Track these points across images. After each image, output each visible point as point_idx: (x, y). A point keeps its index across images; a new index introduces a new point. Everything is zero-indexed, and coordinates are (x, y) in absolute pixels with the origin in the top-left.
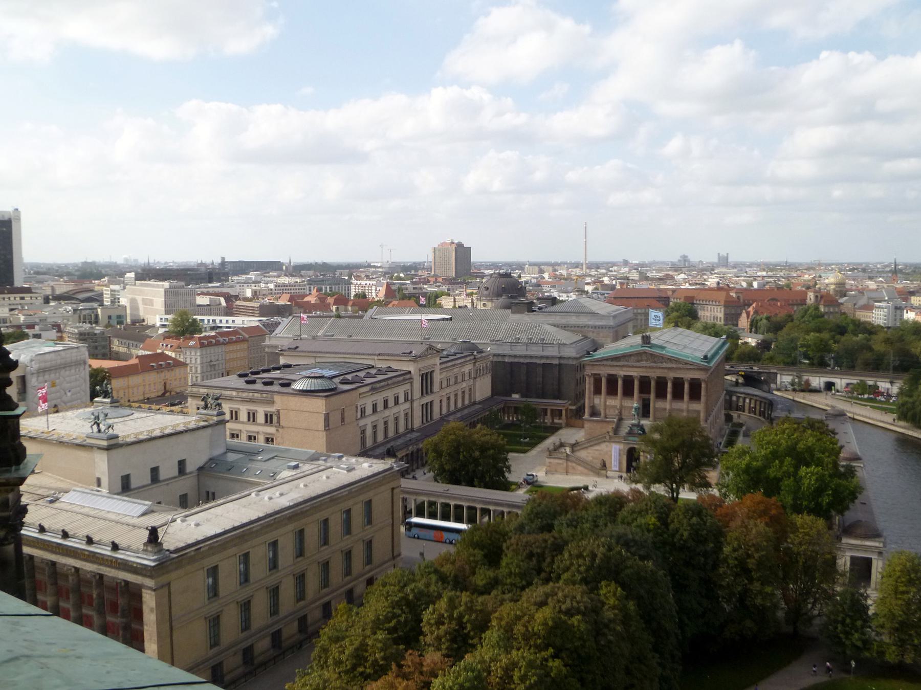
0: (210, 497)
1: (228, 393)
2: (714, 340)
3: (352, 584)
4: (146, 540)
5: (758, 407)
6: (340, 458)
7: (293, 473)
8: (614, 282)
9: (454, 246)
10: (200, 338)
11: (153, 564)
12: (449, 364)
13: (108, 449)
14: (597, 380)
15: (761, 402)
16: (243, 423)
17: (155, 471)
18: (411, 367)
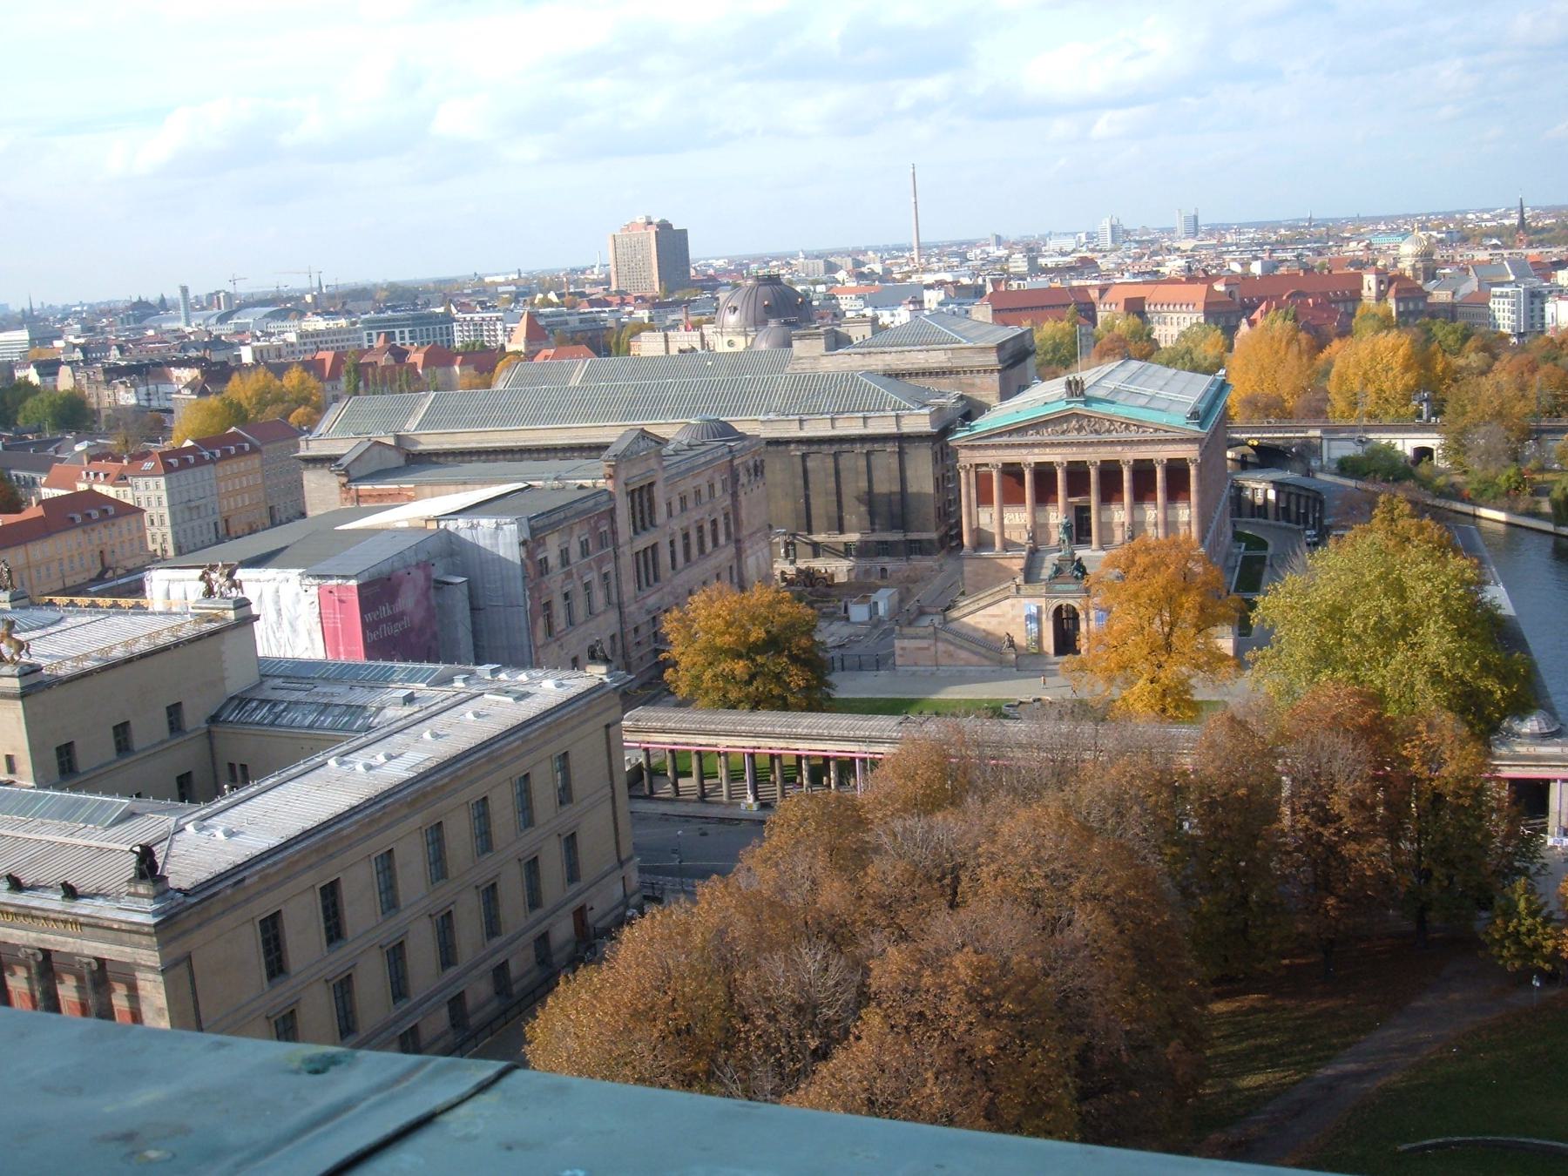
0: (240, 775)
3: (545, 923)
4: (131, 873)
5: (1293, 508)
7: (407, 710)
8: (980, 281)
9: (652, 231)
10: (164, 456)
14: (983, 482)
15: (1299, 496)
17: (122, 732)
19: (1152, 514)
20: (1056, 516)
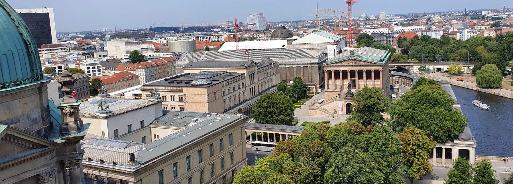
1: (161, 88)
2: (383, 51)
6: (216, 115)
11: (133, 171)
12: (261, 69)
13: (107, 118)
14: (330, 73)
16: (169, 101)
18: (244, 71)
19: (339, 82)
20: (346, 82)
